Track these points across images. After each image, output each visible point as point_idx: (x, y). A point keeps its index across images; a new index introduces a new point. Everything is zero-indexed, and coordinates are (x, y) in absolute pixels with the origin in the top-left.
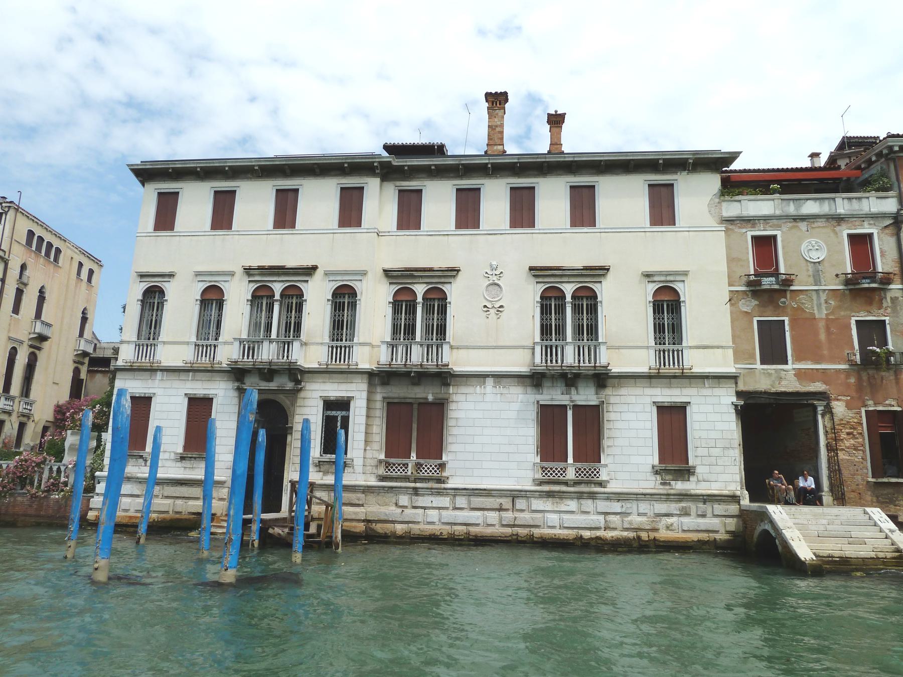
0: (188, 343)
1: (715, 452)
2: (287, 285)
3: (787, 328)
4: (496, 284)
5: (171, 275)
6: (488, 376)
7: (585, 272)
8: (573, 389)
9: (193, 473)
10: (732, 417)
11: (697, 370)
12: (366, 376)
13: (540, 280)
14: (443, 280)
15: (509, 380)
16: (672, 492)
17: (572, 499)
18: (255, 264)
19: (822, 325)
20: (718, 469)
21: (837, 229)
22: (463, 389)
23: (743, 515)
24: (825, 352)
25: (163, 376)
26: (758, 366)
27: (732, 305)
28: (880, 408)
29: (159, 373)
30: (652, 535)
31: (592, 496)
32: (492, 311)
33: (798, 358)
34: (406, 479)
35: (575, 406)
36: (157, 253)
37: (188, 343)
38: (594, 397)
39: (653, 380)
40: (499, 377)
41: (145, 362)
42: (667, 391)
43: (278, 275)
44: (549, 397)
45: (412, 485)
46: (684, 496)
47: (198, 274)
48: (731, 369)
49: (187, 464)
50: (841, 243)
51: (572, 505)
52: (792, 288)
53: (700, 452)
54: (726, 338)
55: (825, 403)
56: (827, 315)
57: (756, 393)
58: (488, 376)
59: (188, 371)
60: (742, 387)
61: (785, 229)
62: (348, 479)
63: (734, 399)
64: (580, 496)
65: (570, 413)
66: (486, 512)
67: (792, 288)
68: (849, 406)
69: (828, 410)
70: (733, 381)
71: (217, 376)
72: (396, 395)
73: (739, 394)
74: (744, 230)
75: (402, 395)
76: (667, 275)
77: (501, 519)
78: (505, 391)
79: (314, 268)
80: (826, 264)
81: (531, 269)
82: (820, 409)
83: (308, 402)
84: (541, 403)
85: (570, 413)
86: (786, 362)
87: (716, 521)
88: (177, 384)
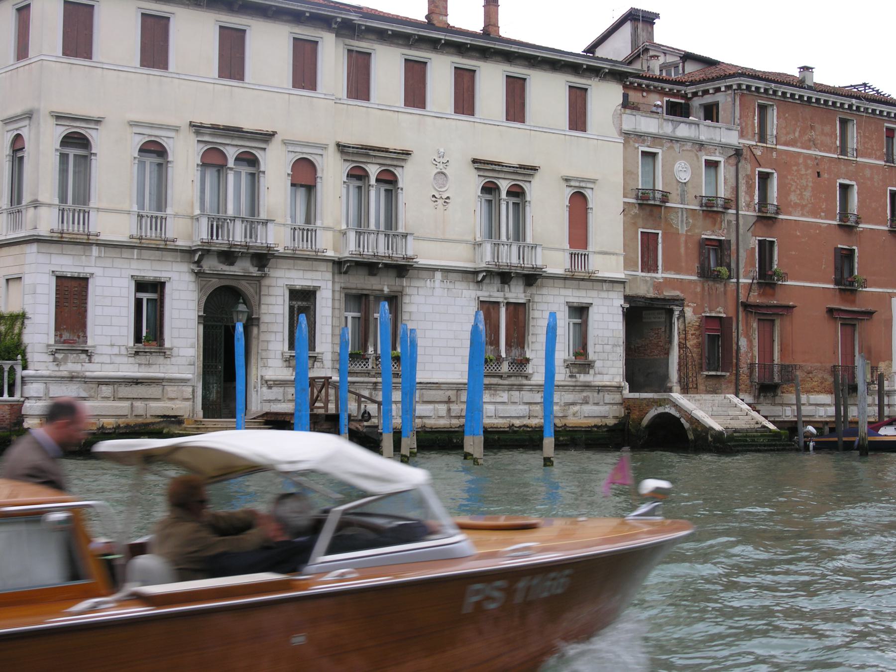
0: (129, 213)
1: (608, 348)
2: (147, 139)
3: (660, 240)
4: (442, 173)
5: (98, 122)
6: (437, 270)
7: (519, 171)
8: (506, 286)
9: (151, 370)
10: (620, 318)
11: (602, 274)
12: (330, 264)
13: (481, 173)
14: (395, 163)
15: (455, 275)
16: (579, 384)
17: (504, 391)
18: (207, 121)
19: (683, 239)
20: (609, 363)
21: (699, 154)
22: (416, 283)
23: (625, 403)
24: (683, 264)
25: (100, 252)
26: (639, 273)
27: (624, 215)
28: (713, 315)
29: (94, 248)
30: (564, 421)
31: (520, 387)
32: (440, 202)
33: (666, 269)
34: (368, 374)
35: (508, 304)
36: (71, 88)
37: (129, 213)
38: (522, 296)
39: (567, 281)
40: (447, 271)
41: (73, 228)
42: (577, 293)
43: (232, 137)
44: (486, 294)
45: (374, 380)
46: (587, 386)
47: (133, 124)
48: (620, 275)
49: (142, 359)
50: (700, 167)
51: (504, 396)
52: (667, 205)
53: (599, 348)
54: (619, 246)
55: (681, 309)
56: (687, 231)
57: (638, 297)
58: (437, 270)
59: (565, 279)
60: (628, 292)
61: (665, 148)
62: (95, 370)
63: (622, 302)
64: (511, 387)
65: (503, 310)
66: (436, 405)
67: (667, 205)
68: (695, 312)
69: (682, 314)
70: (622, 285)
71: (169, 256)
72: (354, 286)
73: (627, 298)
74: (637, 145)
75: (359, 286)
76: (580, 181)
77: (449, 410)
78: (451, 286)
79: (274, 134)
80: (689, 185)
81: (475, 161)
82: (677, 313)
83: (273, 291)
84: (481, 299)
85: (503, 310)
86: (656, 270)
87: (607, 408)
88: (119, 263)
